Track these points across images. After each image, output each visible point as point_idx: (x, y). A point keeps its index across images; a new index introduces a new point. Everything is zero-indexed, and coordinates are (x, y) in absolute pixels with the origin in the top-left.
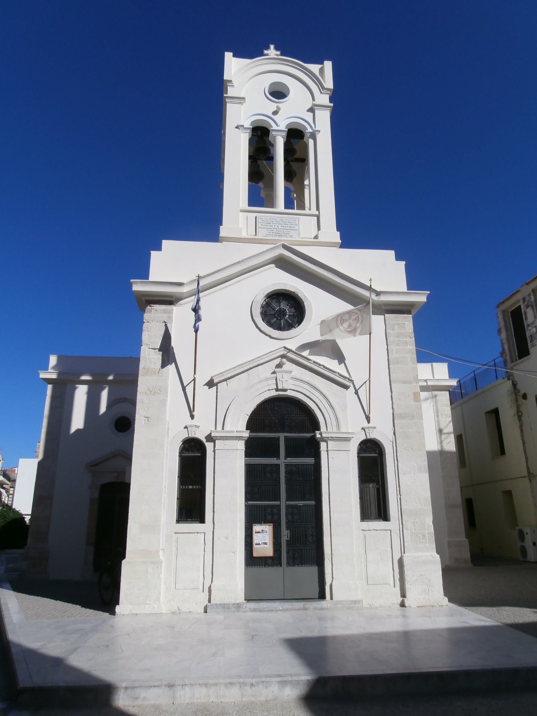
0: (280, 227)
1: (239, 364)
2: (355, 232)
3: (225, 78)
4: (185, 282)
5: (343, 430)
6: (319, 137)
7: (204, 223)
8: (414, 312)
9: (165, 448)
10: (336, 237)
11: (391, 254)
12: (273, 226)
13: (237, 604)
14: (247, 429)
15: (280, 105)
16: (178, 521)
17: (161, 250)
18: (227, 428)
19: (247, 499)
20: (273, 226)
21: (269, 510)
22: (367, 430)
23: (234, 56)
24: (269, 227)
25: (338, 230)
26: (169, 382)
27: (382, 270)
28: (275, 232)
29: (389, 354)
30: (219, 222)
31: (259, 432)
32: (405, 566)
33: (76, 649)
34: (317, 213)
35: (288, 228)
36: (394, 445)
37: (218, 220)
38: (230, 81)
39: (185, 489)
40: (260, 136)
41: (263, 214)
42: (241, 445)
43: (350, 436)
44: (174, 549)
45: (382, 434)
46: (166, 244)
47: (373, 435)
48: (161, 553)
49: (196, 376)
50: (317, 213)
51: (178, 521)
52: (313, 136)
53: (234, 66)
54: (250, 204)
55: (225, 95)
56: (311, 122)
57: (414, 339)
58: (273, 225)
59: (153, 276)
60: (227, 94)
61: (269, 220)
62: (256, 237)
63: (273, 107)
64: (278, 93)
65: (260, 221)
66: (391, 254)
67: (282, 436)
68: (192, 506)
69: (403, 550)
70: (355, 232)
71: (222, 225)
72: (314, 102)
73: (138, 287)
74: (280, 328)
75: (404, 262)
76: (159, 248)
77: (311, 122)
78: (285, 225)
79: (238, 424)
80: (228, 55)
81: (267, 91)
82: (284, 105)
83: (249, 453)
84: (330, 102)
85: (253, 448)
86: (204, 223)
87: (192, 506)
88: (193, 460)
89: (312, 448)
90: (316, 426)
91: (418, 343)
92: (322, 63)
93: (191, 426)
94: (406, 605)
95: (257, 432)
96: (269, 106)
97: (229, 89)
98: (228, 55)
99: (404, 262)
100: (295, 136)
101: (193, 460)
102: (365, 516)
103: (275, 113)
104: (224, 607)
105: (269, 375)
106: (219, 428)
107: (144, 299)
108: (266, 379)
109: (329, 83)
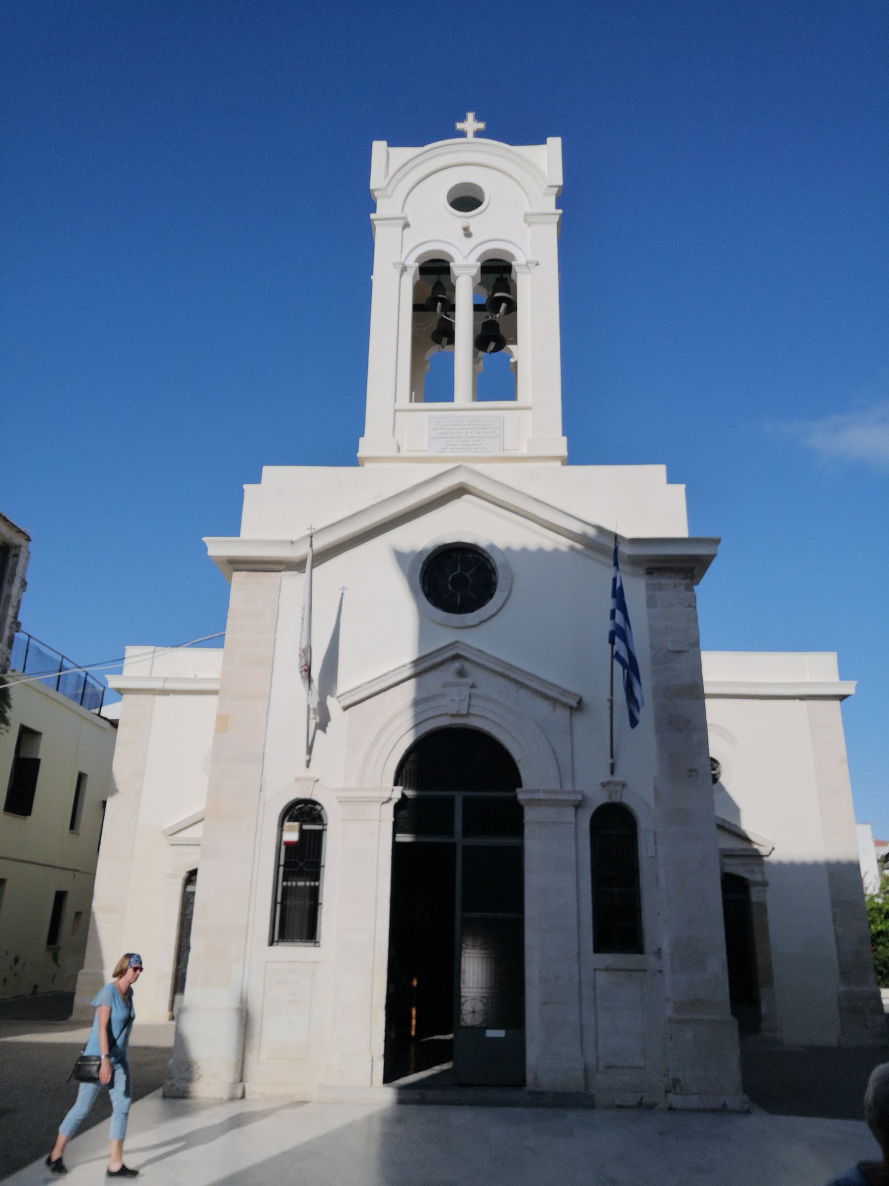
2: (588, 440)
7: (336, 441)
10: (561, 447)
11: (659, 471)
17: (259, 482)
29: (157, 1164)
37: (356, 426)
40: (435, 273)
41: (433, 412)
42: (389, 809)
46: (269, 472)
64: (466, 201)
66: (659, 471)
67: (459, 797)
68: (297, 915)
73: (218, 547)
81: (464, 195)
84: (557, 207)
86: (336, 441)
89: (512, 819)
90: (515, 781)
98: (379, 147)
100: (497, 273)
102: (602, 944)
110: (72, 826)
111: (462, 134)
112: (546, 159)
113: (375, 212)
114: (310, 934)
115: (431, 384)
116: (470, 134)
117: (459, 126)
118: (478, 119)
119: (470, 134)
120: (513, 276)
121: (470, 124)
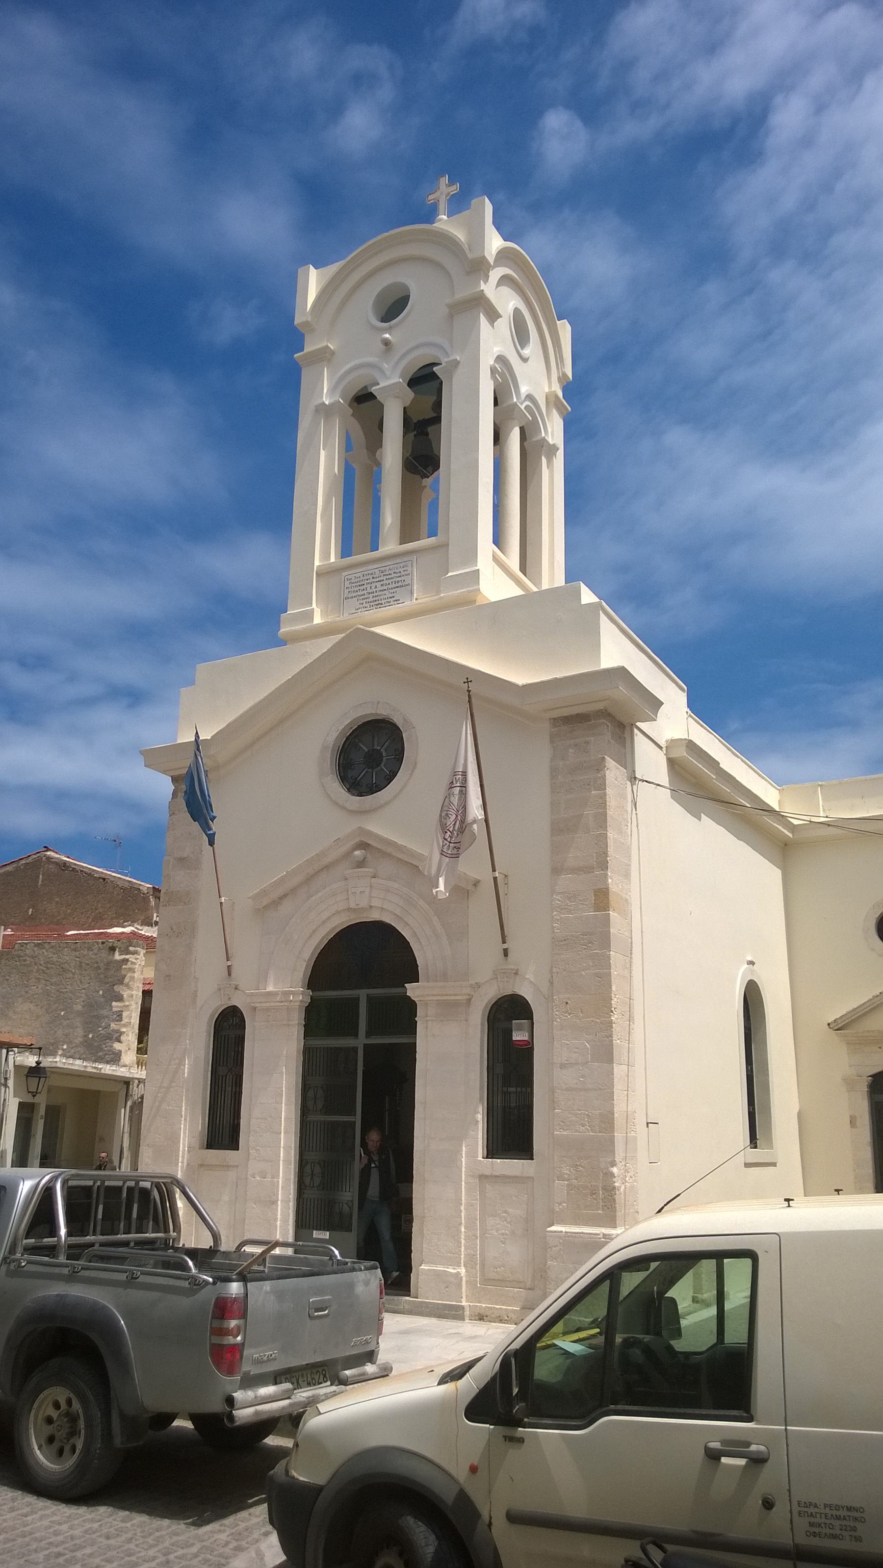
12: (369, 588)
20: (369, 588)
89: (403, 1016)
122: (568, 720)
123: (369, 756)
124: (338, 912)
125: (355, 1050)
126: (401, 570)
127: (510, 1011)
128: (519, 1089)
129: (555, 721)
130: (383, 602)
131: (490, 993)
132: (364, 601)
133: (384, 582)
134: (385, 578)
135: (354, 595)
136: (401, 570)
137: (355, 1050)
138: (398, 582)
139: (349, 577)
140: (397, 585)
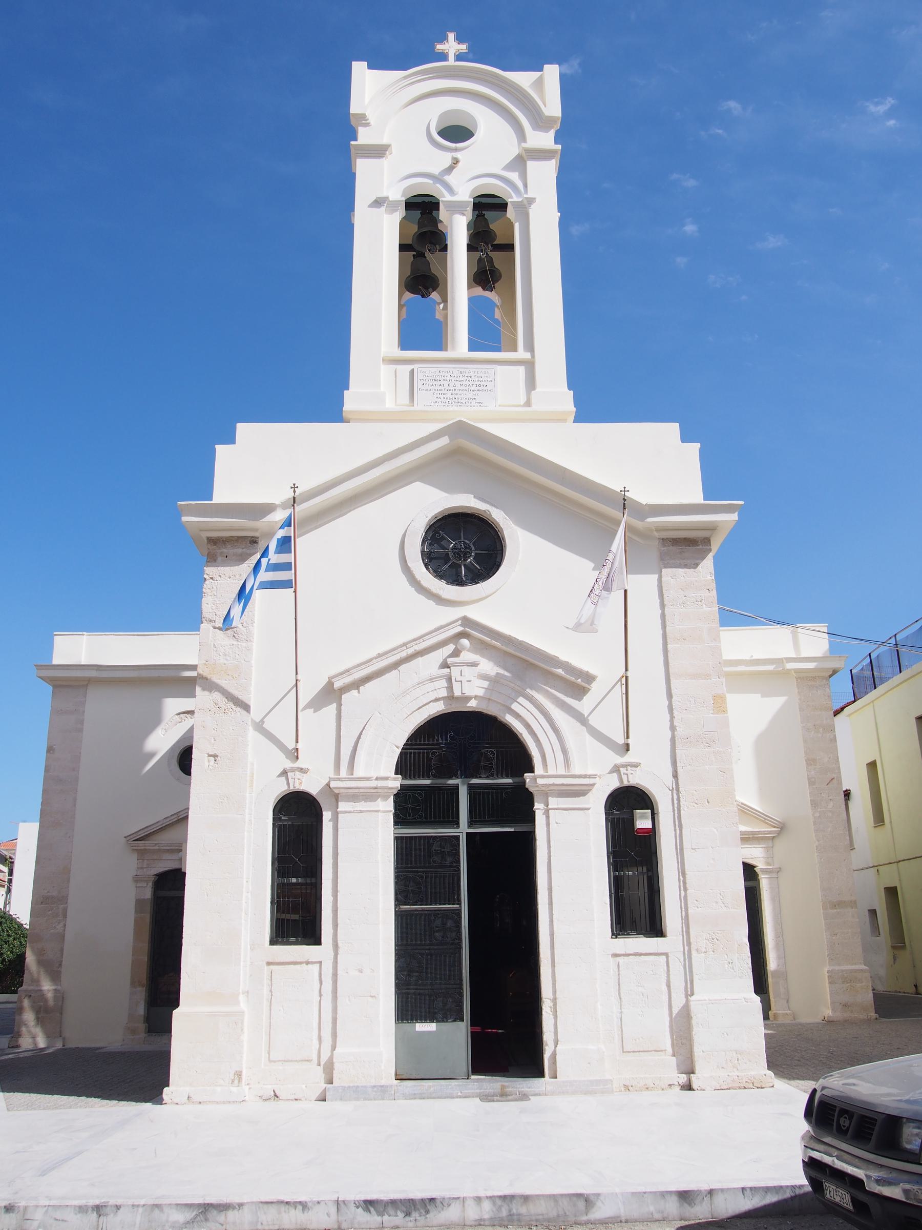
0: (458, 387)
1: (381, 651)
2: (601, 393)
3: (354, 109)
4: (277, 503)
5: (576, 771)
6: (533, 211)
7: (317, 391)
8: (715, 545)
9: (247, 811)
10: (566, 401)
11: (675, 427)
12: (446, 385)
13: (382, 1086)
14: (396, 773)
15: (458, 155)
16: (273, 942)
18: (359, 772)
19: (398, 901)
20: (446, 385)
21: (438, 922)
22: (623, 770)
23: (370, 67)
24: (437, 387)
25: (569, 389)
26: (252, 689)
27: (652, 464)
28: (450, 396)
30: (345, 384)
31: (419, 778)
32: (694, 1018)
33: (79, 1153)
34: (527, 356)
35: (474, 388)
36: (675, 797)
37: (340, 378)
38: (362, 117)
39: (284, 884)
40: (423, 210)
42: (388, 806)
43: (591, 781)
44: (266, 991)
45: (650, 777)
46: (243, 429)
47: (635, 779)
48: (242, 998)
49: (299, 746)
50: (527, 356)
51: (273, 942)
52: (523, 209)
53: (371, 90)
54: (405, 344)
55: (352, 143)
56: (520, 185)
57: (714, 593)
58: (446, 383)
59: (222, 494)
60: (356, 140)
61: (438, 374)
62: (412, 408)
63: (445, 159)
65: (421, 376)
68: (297, 915)
69: (689, 992)
70: (601, 393)
71: (370, 67)
72: (524, 145)
74: (457, 581)
75: (698, 445)
76: (230, 439)
77: (520, 185)
78: (468, 383)
79: (380, 766)
80: (359, 68)
81: (412, 128)
82: (468, 152)
83: (400, 819)
85: (408, 807)
86: (317, 391)
87: (297, 915)
88: (299, 827)
89: (520, 806)
91: (721, 599)
92: (541, 69)
93: (293, 770)
94: (694, 1086)
95: (415, 778)
96: (437, 160)
97: (361, 131)
98: (359, 68)
99: (698, 445)
100: (489, 213)
101: (299, 827)
103: (450, 169)
104: (357, 1093)
105: (435, 670)
106: (344, 773)
107: (205, 535)
108: (431, 680)
109: (553, 106)
110: (626, 591)
111: (443, 57)
112: (546, 85)
113: (356, 140)
114: (312, 936)
115: (420, 334)
116: (451, 57)
117: (440, 47)
118: (459, 40)
119: (451, 57)
120: (440, 227)
121: (451, 46)
122: (676, 542)
123: (464, 548)
124: (437, 700)
125: (457, 838)
126: (483, 375)
127: (627, 802)
128: (308, 881)
129: (664, 541)
130: (464, 401)
131: (608, 785)
132: (442, 397)
133: (464, 383)
134: (464, 379)
135: (430, 388)
136: (483, 375)
137: (457, 838)
138: (480, 386)
139: (423, 370)
140: (478, 388)
